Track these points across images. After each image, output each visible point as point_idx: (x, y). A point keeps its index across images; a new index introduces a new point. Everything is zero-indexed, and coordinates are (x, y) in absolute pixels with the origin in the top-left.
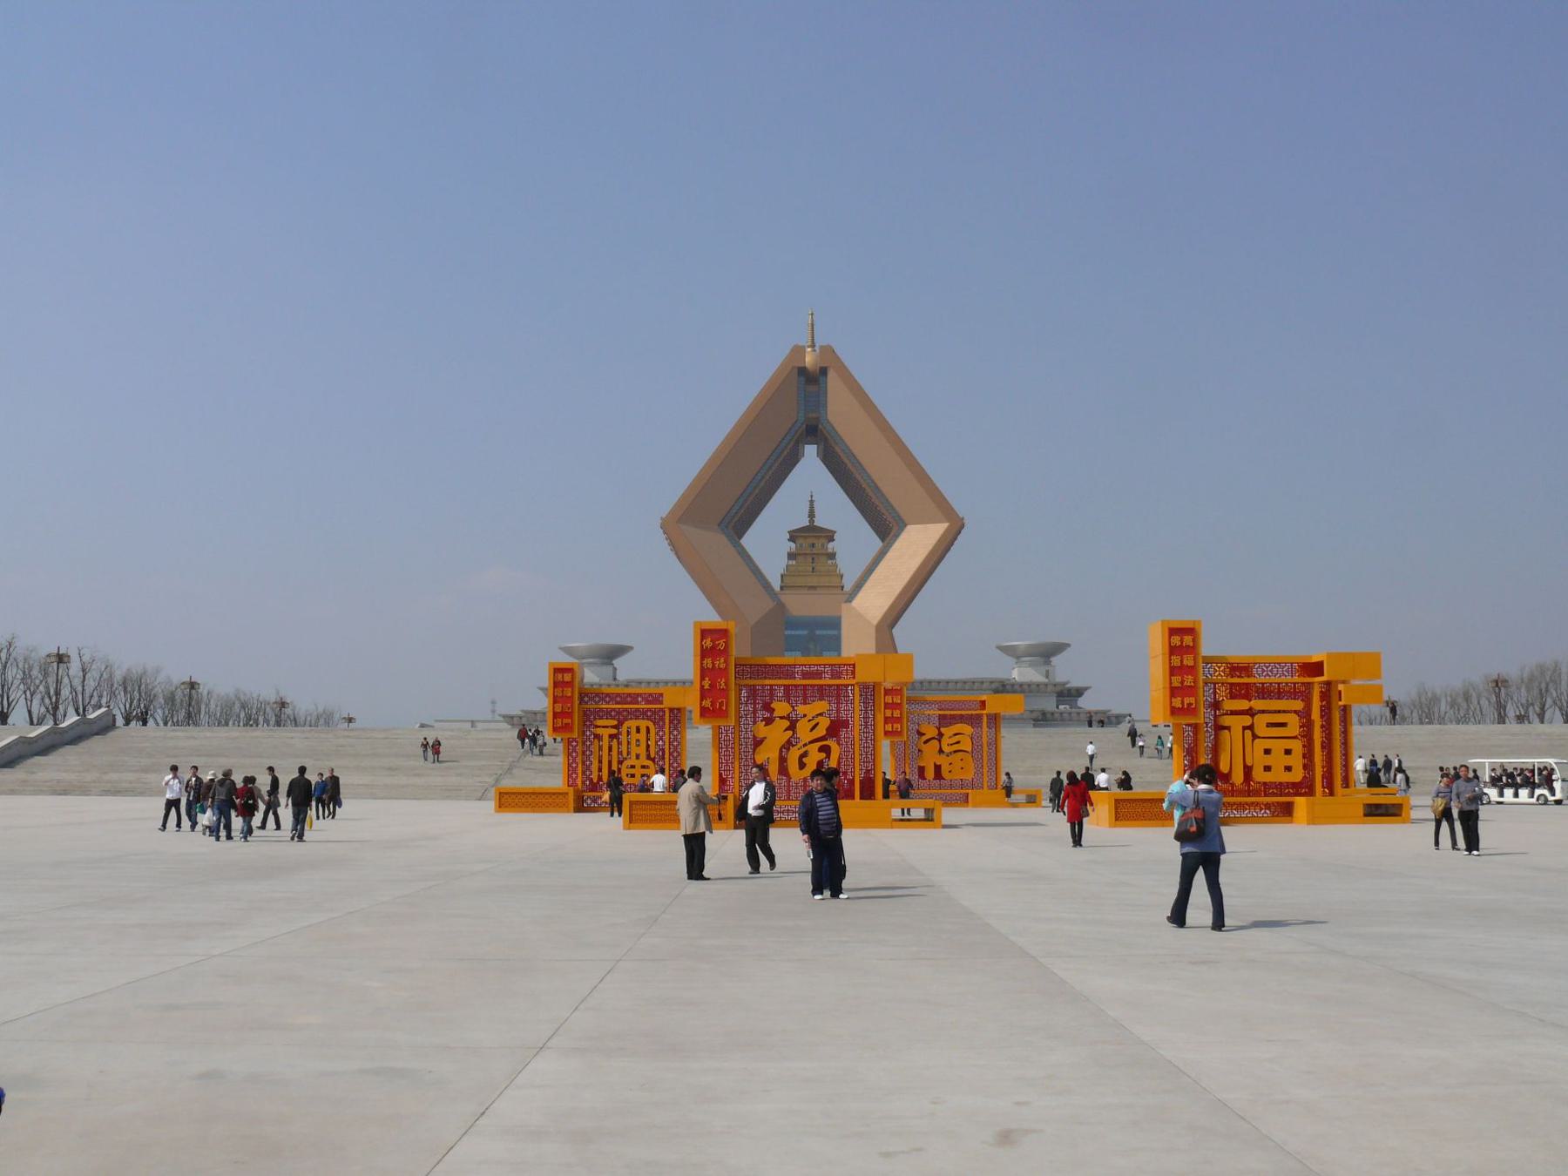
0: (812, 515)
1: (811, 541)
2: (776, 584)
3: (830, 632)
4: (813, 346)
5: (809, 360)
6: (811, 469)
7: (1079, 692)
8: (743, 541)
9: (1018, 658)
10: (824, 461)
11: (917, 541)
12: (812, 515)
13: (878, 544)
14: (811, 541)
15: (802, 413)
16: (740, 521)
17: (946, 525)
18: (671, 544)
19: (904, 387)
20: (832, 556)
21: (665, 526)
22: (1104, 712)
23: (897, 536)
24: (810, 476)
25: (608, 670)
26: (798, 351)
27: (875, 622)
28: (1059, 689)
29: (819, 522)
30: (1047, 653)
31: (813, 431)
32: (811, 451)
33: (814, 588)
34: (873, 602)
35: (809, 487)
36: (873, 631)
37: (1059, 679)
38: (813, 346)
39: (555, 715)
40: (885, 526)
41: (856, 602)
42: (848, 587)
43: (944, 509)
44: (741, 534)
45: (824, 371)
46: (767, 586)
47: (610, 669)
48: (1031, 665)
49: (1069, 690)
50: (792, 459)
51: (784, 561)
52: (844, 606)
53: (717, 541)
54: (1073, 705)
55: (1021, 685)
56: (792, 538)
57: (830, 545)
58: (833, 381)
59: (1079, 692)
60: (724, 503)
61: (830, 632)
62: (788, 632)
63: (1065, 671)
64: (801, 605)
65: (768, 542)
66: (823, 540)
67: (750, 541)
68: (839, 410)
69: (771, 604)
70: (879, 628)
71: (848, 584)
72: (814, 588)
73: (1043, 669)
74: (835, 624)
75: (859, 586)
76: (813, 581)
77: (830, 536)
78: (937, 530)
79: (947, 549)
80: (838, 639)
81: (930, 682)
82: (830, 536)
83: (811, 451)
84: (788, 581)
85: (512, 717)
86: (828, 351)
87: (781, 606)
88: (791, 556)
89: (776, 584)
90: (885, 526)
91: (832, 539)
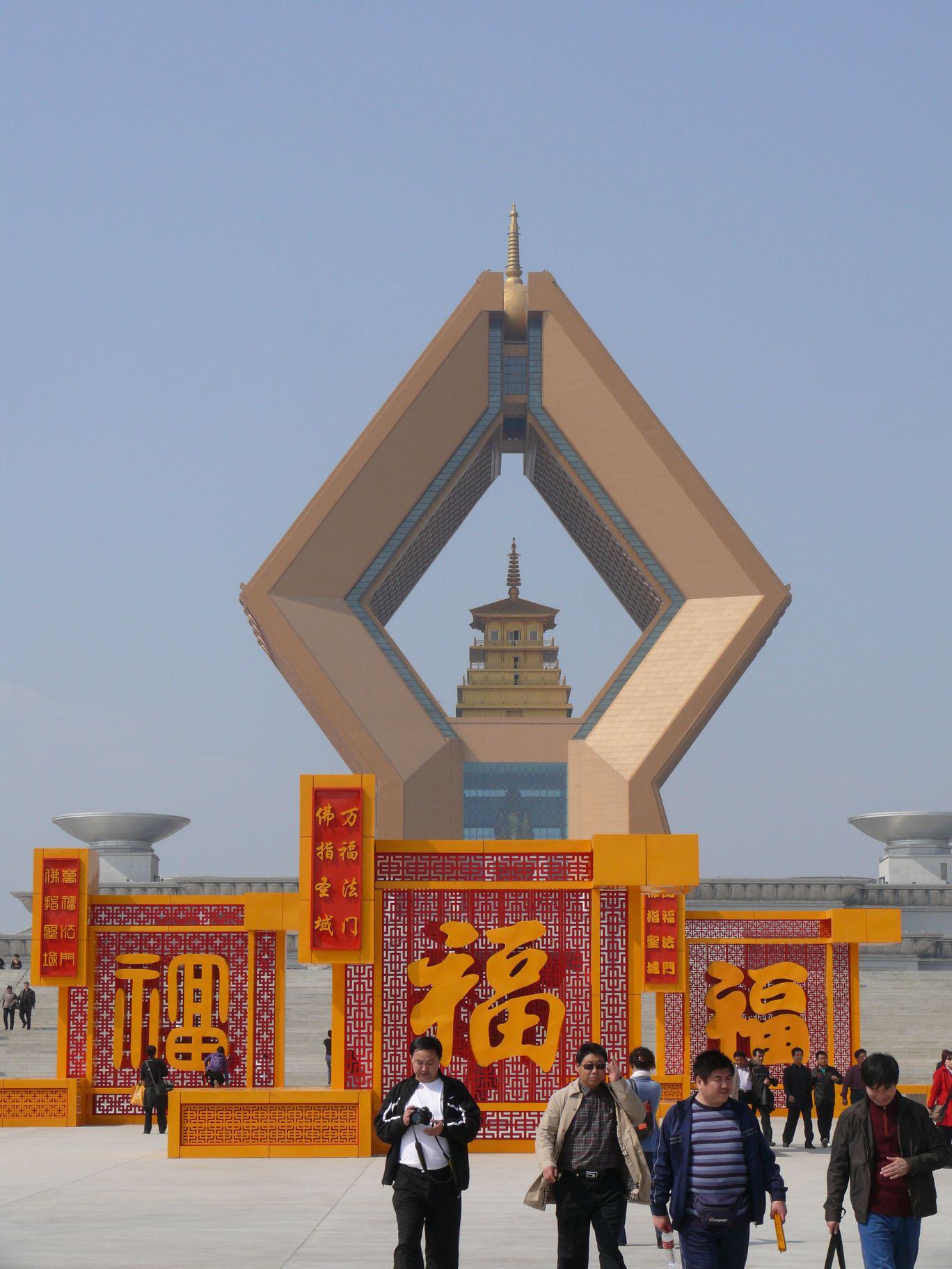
0: (514, 580)
1: (513, 627)
11: (704, 628)
12: (514, 580)
14: (513, 627)
17: (757, 599)
26: (490, 282)
27: (628, 775)
29: (525, 594)
32: (512, 463)
35: (510, 529)
41: (593, 739)
43: (757, 572)
44: (384, 624)
46: (433, 709)
50: (478, 480)
52: (573, 745)
62: (472, 793)
65: (434, 629)
66: (534, 626)
70: (634, 783)
71: (580, 705)
75: (598, 709)
77: (547, 618)
82: (547, 618)
83: (512, 463)
86: (544, 282)
87: (457, 746)
89: (449, 706)
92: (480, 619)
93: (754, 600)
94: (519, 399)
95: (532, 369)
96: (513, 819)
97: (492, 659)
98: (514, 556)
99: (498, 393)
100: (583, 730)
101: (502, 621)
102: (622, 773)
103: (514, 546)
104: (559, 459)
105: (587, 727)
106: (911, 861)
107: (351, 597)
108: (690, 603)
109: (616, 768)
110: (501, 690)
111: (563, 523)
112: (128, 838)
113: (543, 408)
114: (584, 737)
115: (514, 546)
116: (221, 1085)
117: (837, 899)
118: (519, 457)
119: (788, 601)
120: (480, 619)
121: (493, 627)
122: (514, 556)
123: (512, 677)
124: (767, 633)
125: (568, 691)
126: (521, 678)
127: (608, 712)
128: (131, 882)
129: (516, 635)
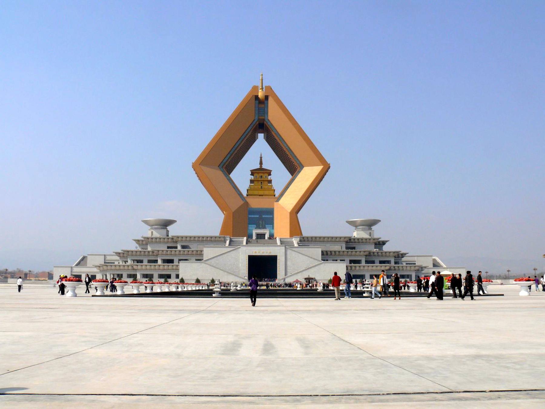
0: (261, 163)
1: (261, 175)
2: (245, 193)
3: (270, 216)
4: (262, 89)
5: (261, 94)
6: (261, 144)
7: (384, 243)
8: (231, 176)
9: (356, 226)
11: (308, 174)
12: (261, 163)
13: (290, 176)
14: (261, 175)
15: (256, 120)
16: (229, 165)
17: (322, 167)
18: (200, 179)
19: (302, 106)
20: (270, 182)
21: (194, 166)
22: (398, 252)
23: (299, 172)
25: (164, 231)
26: (255, 88)
27: (289, 211)
28: (376, 241)
30: (370, 224)
31: (262, 126)
32: (261, 136)
33: (262, 195)
34: (288, 201)
35: (260, 151)
37: (376, 236)
38: (262, 89)
39: (382, 253)
40: (293, 167)
41: (281, 202)
43: (322, 160)
44: (230, 173)
45: (267, 97)
46: (240, 194)
47: (165, 231)
48: (363, 230)
49: (379, 242)
50: (252, 140)
51: (248, 183)
52: (275, 203)
53: (219, 174)
54: (381, 249)
55: (358, 239)
56: (252, 174)
57: (269, 177)
58: (271, 102)
59: (384, 243)
60: (224, 156)
61: (270, 216)
63: (378, 232)
64: (256, 203)
65: (241, 177)
66: (267, 175)
68: (274, 116)
69: (242, 202)
70: (291, 213)
71: (277, 194)
72: (262, 195)
74: (271, 212)
75: (282, 195)
76: (261, 192)
77: (269, 173)
78: (318, 169)
79: (321, 180)
80: (272, 219)
81: (316, 238)
82: (269, 173)
83: (261, 136)
84: (250, 192)
85: (139, 241)
86: (269, 88)
87: (247, 203)
88: (252, 181)
89: (245, 193)
90: (293, 167)
91: (270, 174)
92: (253, 173)
94: (262, 118)
96: (261, 222)
98: (261, 157)
100: (278, 199)
101: (258, 173)
106: (362, 232)
108: (305, 168)
119: (329, 168)
120: (253, 173)
121: (255, 175)
122: (261, 157)
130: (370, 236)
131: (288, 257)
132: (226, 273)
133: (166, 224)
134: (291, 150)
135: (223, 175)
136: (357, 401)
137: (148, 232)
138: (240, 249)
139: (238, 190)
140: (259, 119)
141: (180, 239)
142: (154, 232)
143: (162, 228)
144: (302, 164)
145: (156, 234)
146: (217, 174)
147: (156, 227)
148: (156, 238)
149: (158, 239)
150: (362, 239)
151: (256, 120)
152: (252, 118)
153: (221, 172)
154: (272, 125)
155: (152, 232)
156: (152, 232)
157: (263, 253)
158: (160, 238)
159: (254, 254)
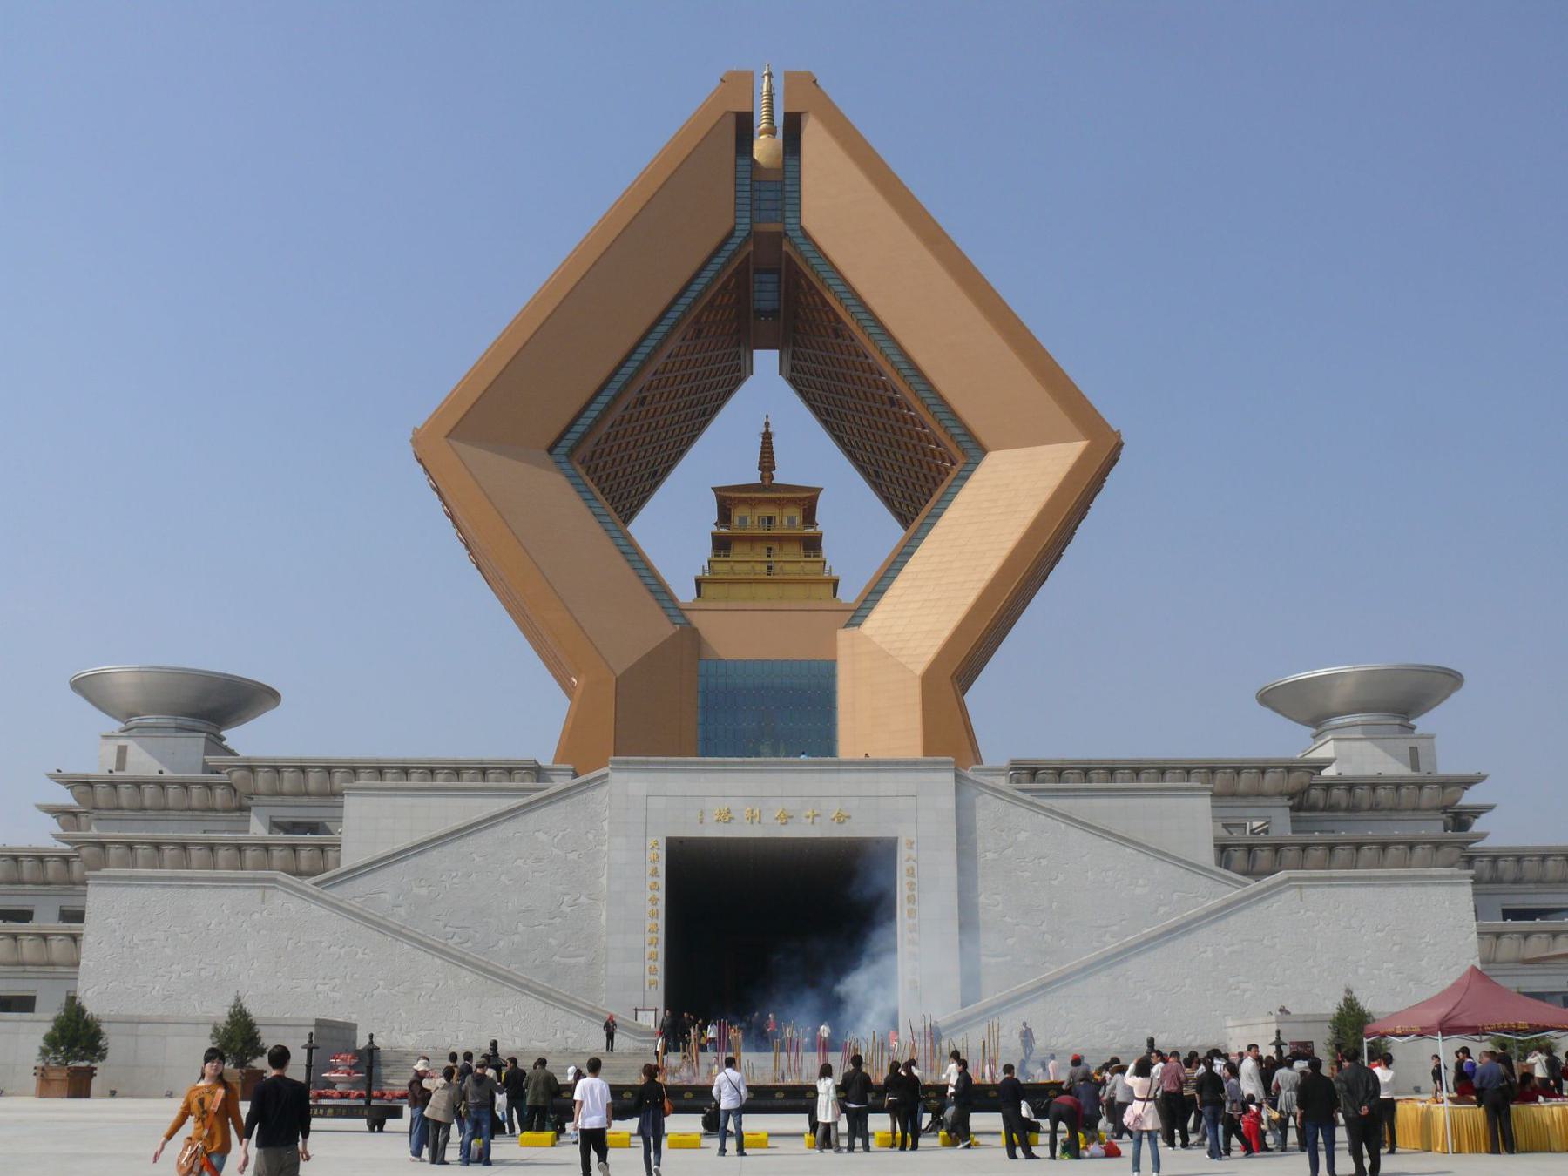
0: (767, 461)
1: (766, 527)
10: (793, 381)
11: (1000, 497)
12: (767, 461)
13: (895, 532)
16: (619, 454)
17: (1081, 445)
23: (964, 478)
24: (766, 397)
27: (919, 669)
28: (1296, 780)
29: (780, 477)
30: (1404, 699)
32: (766, 361)
35: (764, 418)
36: (918, 683)
42: (849, 594)
43: (1080, 413)
44: (628, 518)
46: (659, 591)
50: (736, 375)
52: (843, 635)
63: (1451, 739)
64: (744, 635)
65: (675, 527)
67: (642, 527)
68: (836, 213)
71: (849, 594)
73: (1404, 744)
75: (876, 592)
83: (766, 361)
86: (803, 82)
87: (690, 639)
88: (721, 544)
89: (685, 593)
93: (1078, 447)
94: (774, 227)
95: (788, 188)
97: (739, 552)
98: (767, 438)
99: (747, 220)
100: (857, 615)
102: (911, 667)
103: (767, 425)
104: (829, 298)
105: (863, 612)
106: (1367, 745)
107: (558, 450)
109: (903, 660)
110: (750, 582)
111: (826, 424)
112: (174, 713)
113: (802, 229)
114: (859, 625)
115: (767, 425)
116: (1249, 1150)
117: (1281, 794)
118: (774, 355)
119: (1119, 446)
120: (728, 501)
122: (767, 438)
123: (764, 567)
124: (1080, 510)
125: (836, 583)
126: (776, 567)
127: (890, 592)
128: (167, 773)
129: (770, 519)
130: (1415, 766)
131: (987, 853)
132: (467, 977)
133: (220, 703)
134: (915, 368)
135: (572, 492)
136: (581, 792)
137: (92, 745)
138: (600, 794)
139: (649, 567)
140: (753, 235)
141: (263, 780)
142: (133, 747)
143: (180, 729)
144: (968, 433)
145: (143, 762)
146: (555, 497)
147: (150, 720)
148: (138, 785)
149: (148, 792)
150: (1374, 787)
151: (741, 234)
152: (717, 216)
153: (561, 479)
154: (817, 248)
155: (122, 751)
156: (122, 751)
157: (786, 819)
158: (162, 786)
159: (712, 831)
